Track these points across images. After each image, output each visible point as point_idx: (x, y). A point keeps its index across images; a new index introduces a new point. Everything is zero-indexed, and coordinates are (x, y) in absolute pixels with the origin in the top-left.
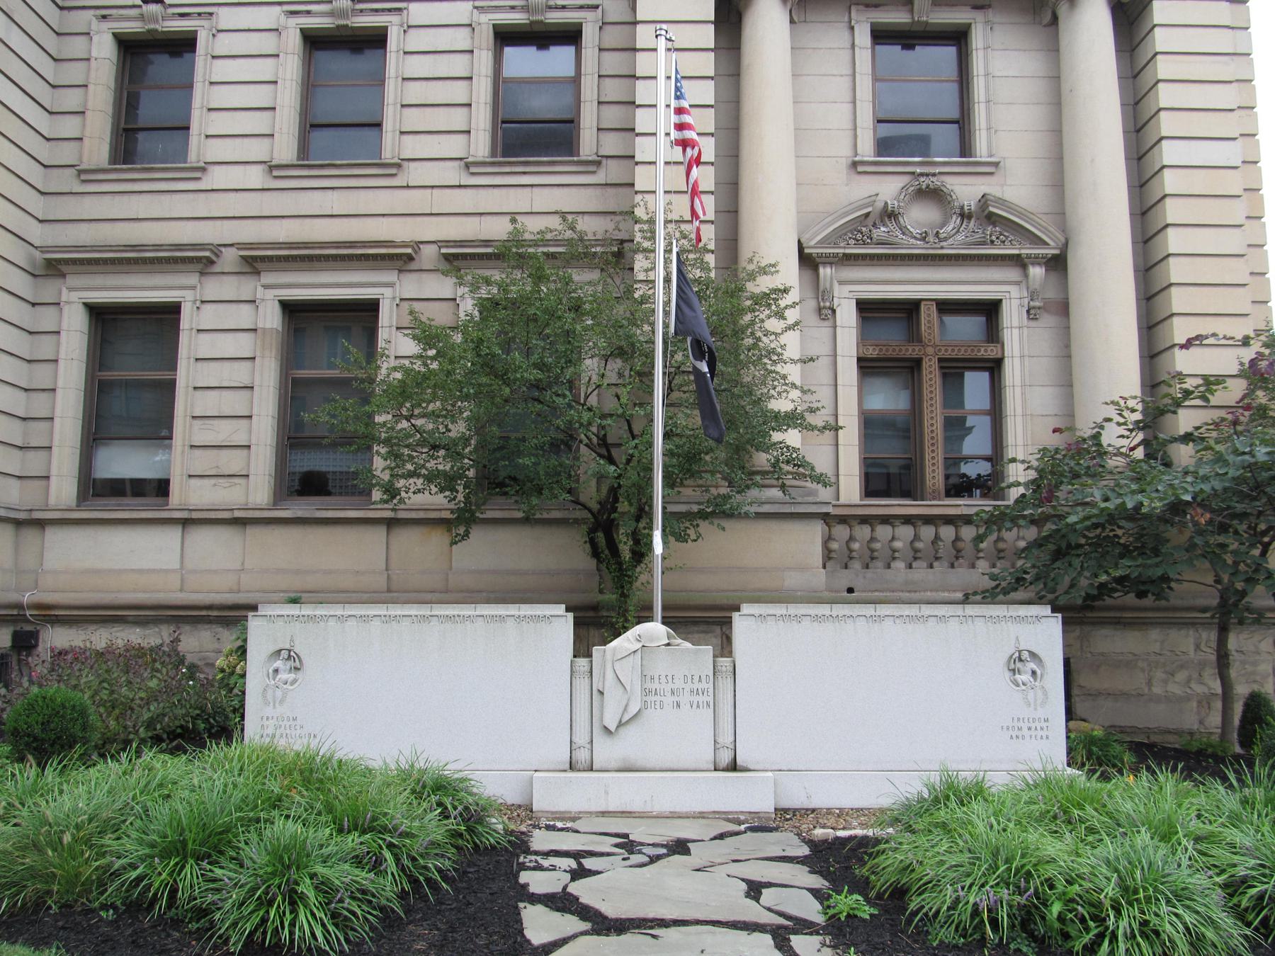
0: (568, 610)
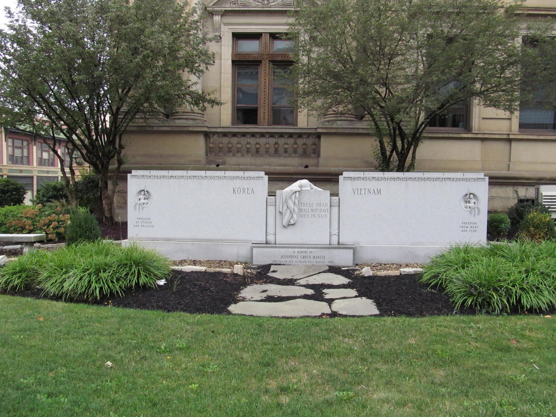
0: (266, 174)
